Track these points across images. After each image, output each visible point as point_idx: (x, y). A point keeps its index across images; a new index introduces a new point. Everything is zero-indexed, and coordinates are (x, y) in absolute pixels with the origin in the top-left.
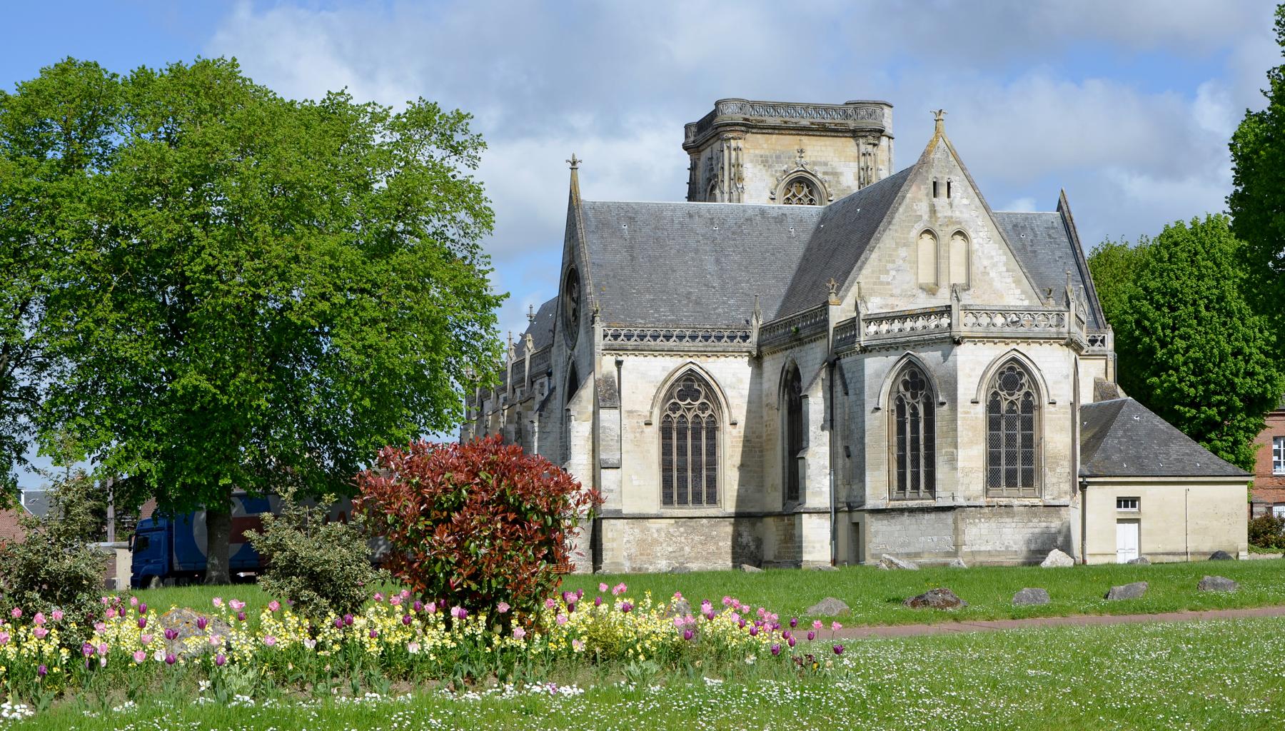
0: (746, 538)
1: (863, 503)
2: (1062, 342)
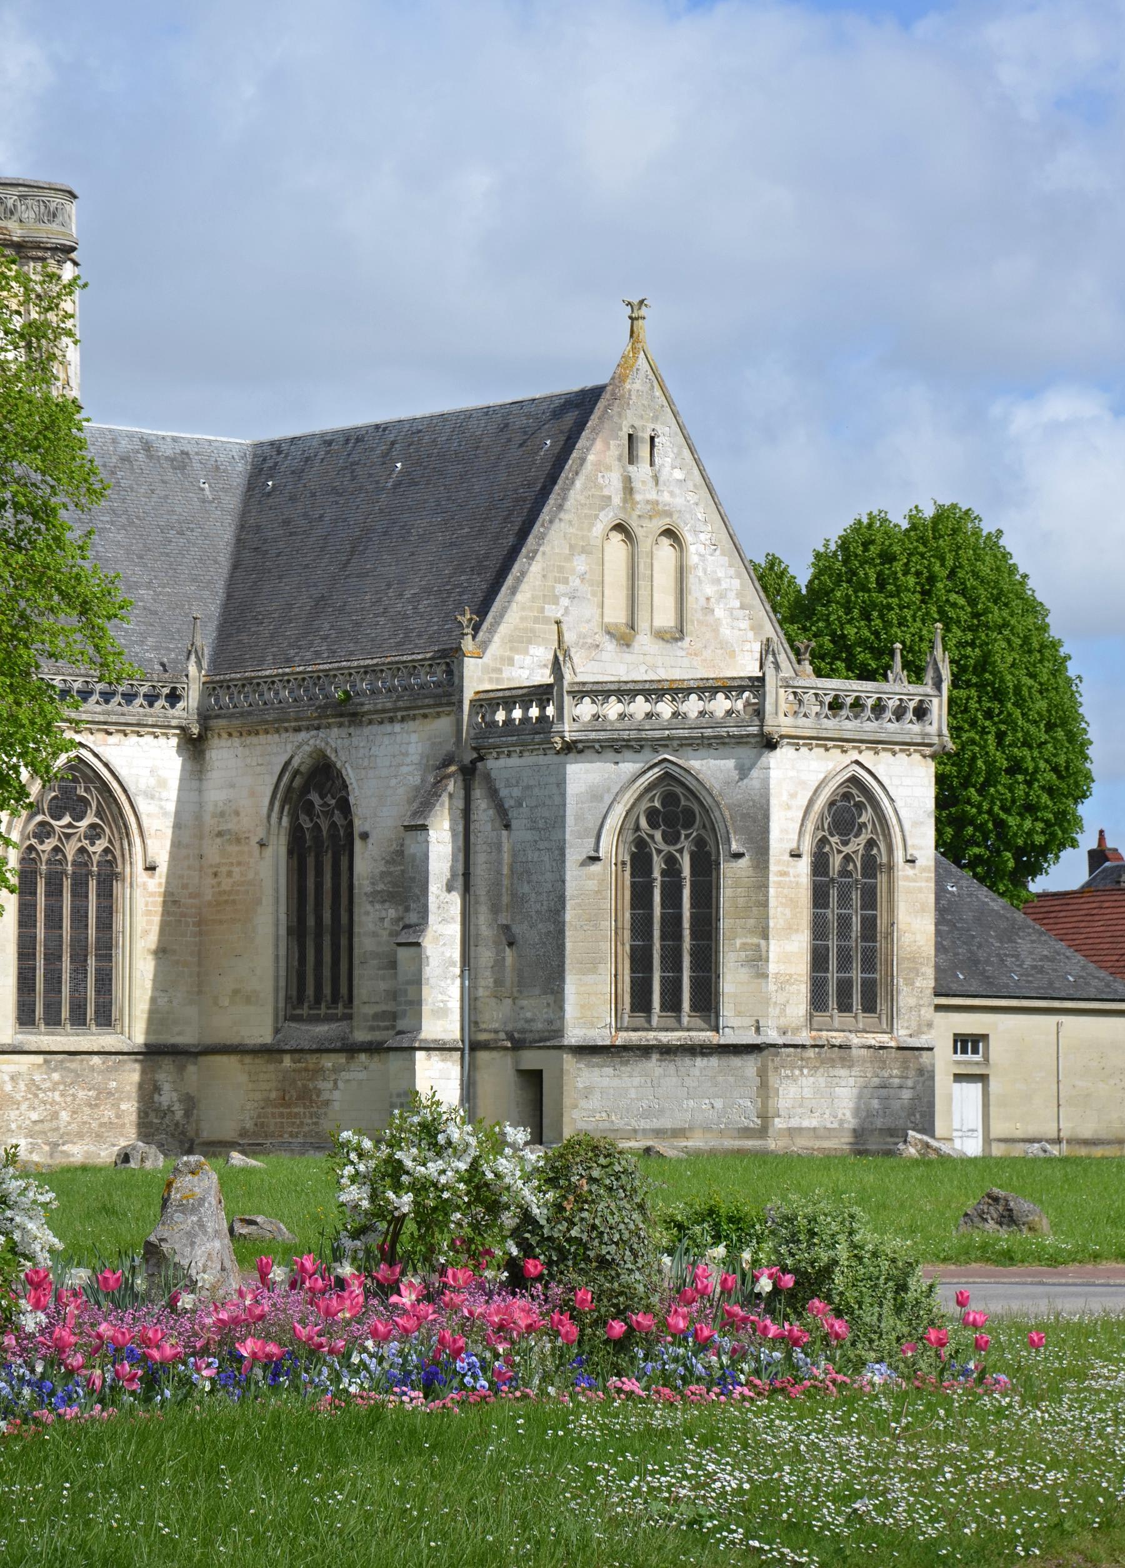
0: (167, 1097)
1: (559, 1033)
2: (928, 751)
